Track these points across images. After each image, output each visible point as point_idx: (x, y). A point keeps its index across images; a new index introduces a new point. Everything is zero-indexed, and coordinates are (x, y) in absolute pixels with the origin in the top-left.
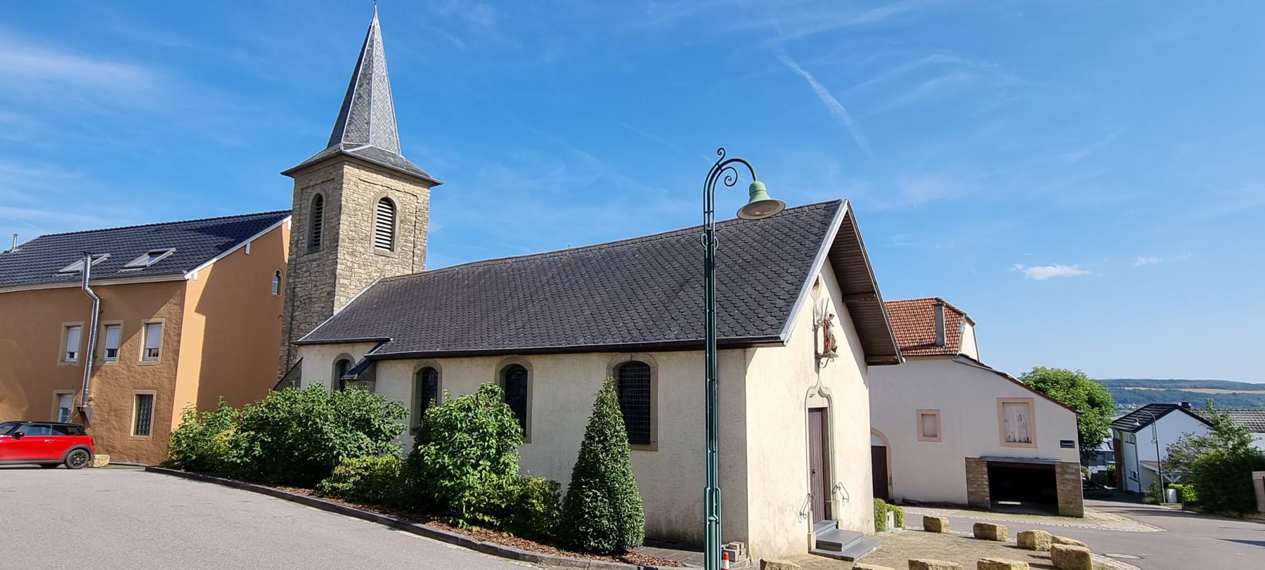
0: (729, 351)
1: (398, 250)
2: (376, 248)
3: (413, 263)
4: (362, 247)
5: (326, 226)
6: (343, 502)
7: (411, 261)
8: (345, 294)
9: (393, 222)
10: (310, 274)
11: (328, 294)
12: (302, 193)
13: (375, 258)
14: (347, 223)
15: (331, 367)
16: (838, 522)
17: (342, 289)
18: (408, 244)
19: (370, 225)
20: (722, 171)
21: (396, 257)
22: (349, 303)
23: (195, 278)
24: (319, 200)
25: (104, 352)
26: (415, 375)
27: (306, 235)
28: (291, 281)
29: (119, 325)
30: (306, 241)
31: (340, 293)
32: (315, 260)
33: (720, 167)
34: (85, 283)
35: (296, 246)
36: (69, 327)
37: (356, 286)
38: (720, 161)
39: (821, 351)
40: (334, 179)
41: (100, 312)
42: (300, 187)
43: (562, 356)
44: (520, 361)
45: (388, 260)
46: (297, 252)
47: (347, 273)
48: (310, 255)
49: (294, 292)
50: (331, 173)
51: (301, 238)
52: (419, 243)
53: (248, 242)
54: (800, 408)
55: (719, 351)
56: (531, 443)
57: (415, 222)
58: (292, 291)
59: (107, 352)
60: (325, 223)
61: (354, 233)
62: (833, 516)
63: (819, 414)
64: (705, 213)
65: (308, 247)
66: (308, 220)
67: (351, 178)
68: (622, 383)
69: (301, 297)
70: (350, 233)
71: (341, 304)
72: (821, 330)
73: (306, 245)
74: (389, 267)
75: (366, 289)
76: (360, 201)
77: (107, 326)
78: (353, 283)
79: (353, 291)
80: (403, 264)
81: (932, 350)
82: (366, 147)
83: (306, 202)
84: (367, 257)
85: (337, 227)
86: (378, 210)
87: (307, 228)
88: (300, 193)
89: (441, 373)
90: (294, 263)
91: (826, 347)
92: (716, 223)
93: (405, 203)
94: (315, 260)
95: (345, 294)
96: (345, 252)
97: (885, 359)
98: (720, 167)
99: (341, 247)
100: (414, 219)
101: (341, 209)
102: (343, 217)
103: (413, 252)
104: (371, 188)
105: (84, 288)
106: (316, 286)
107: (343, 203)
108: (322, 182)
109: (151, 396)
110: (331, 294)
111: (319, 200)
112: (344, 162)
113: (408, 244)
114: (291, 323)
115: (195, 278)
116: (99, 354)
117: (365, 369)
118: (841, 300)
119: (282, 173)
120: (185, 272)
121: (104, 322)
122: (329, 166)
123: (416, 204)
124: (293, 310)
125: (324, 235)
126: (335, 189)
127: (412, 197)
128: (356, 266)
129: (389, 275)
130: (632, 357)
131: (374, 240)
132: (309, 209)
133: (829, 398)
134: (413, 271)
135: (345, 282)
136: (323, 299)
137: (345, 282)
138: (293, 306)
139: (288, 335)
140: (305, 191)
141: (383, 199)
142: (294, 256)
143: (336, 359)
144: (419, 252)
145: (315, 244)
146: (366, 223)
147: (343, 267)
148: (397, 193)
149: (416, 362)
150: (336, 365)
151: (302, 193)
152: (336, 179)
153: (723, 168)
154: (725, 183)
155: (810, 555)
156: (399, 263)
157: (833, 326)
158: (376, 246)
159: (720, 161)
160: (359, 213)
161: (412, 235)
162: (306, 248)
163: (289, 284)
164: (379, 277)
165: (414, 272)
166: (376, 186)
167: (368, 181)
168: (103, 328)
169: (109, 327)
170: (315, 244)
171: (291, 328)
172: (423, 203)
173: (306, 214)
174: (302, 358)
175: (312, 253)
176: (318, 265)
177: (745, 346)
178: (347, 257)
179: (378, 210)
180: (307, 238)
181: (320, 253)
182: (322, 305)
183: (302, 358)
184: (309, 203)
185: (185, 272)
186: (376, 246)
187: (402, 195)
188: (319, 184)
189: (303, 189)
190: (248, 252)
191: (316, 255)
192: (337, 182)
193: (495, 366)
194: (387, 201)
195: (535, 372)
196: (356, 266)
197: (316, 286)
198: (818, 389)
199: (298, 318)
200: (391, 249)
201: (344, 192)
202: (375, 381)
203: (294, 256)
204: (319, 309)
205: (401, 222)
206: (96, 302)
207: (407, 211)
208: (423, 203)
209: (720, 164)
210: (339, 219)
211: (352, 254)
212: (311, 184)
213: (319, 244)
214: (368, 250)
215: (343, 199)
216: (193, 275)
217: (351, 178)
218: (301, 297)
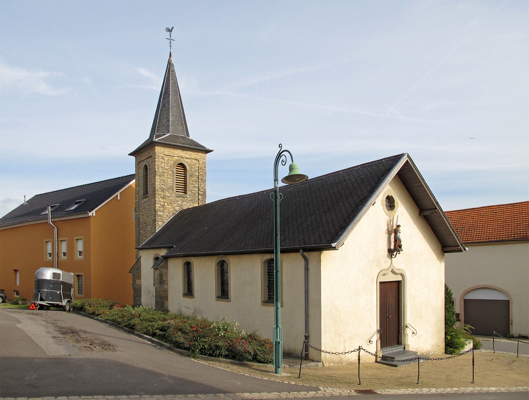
0: (314, 252)
1: (189, 192)
2: (177, 193)
3: (199, 200)
4: (169, 193)
5: (150, 183)
6: (46, 323)
7: (197, 199)
8: (161, 220)
9: (185, 177)
10: (145, 210)
11: (153, 221)
12: (139, 165)
13: (176, 199)
14: (159, 180)
15: (152, 260)
16: (405, 346)
17: (160, 218)
18: (195, 189)
19: (172, 180)
20: (281, 157)
21: (189, 197)
22: (164, 225)
23: (94, 215)
24: (146, 168)
25: (61, 254)
26: (183, 265)
27: (142, 188)
28: (137, 214)
29: (66, 240)
30: (142, 192)
31: (159, 220)
32: (146, 202)
33: (280, 155)
34: (49, 220)
35: (138, 195)
36: (47, 242)
37: (167, 216)
38: (280, 151)
39: (392, 247)
40: (151, 156)
41: (58, 234)
42: (137, 162)
43: (242, 256)
44: (225, 258)
45: (183, 199)
46: (139, 198)
47: (162, 208)
48: (145, 200)
49: (139, 220)
50: (150, 153)
51: (140, 190)
52: (201, 188)
53: (118, 193)
54: (372, 282)
55: (281, 254)
56: (231, 302)
57: (198, 175)
58: (138, 219)
59: (63, 254)
60: (149, 181)
61: (163, 186)
62: (403, 343)
63: (397, 283)
64: (274, 180)
65: (143, 195)
66: (142, 180)
67: (160, 154)
68: (269, 270)
69: (142, 222)
70: (161, 186)
71: (160, 225)
72: (393, 235)
73: (142, 194)
74: (185, 203)
75: (172, 217)
76: (166, 167)
77: (61, 241)
78: (165, 214)
79: (165, 219)
80: (193, 201)
81: (495, 239)
82: (168, 135)
83: (141, 169)
84: (172, 199)
85: (154, 184)
86: (176, 171)
87: (142, 184)
88: (138, 164)
89: (193, 264)
90: (138, 204)
91: (395, 246)
92: (279, 187)
93: (192, 165)
94: (146, 202)
95: (161, 220)
96: (160, 197)
97: (453, 248)
98: (280, 155)
99: (157, 194)
100: (198, 174)
101: (155, 173)
102: (157, 178)
103: (198, 193)
104: (171, 159)
105: (50, 222)
106: (148, 216)
107: (156, 169)
108: (147, 158)
109: (82, 275)
110: (155, 221)
111: (146, 168)
112: (155, 146)
113: (195, 189)
114: (139, 237)
115: (94, 215)
116: (59, 255)
117: (162, 262)
118: (419, 214)
119: (129, 155)
120: (88, 212)
121: (60, 239)
122: (149, 149)
123: (198, 165)
124: (139, 229)
125: (149, 188)
126: (152, 162)
127: (195, 161)
128: (166, 204)
129: (185, 208)
130: (271, 256)
131: (175, 188)
132: (142, 174)
133: (402, 275)
134: (199, 204)
135: (161, 213)
136: (151, 223)
137: (161, 213)
138: (139, 228)
139: (138, 243)
140: (140, 163)
141: (179, 164)
142: (137, 200)
143: (153, 258)
144: (202, 193)
145: (146, 192)
146: (170, 180)
147: (159, 205)
148: (187, 160)
149: (183, 258)
150: (154, 259)
151: (139, 165)
152: (152, 156)
153: (281, 155)
154: (283, 165)
155: (376, 363)
156: (190, 200)
157: (400, 233)
158: (176, 192)
159: (280, 151)
160: (166, 174)
161: (197, 183)
162: (142, 195)
163: (136, 216)
164: (179, 209)
165: (200, 205)
166: (175, 157)
167: (169, 155)
168: (59, 242)
169: (62, 242)
170: (146, 192)
171: (139, 239)
172: (202, 164)
173: (141, 177)
174: (141, 256)
175: (145, 198)
176: (148, 205)
177: (320, 249)
178: (161, 199)
179: (176, 171)
180: (142, 190)
181: (148, 198)
182: (151, 227)
183: (141, 256)
184: (142, 170)
185: (88, 212)
186: (176, 192)
187: (190, 161)
188: (145, 159)
189: (139, 163)
190: (119, 199)
191: (146, 199)
192: (152, 157)
193: (214, 261)
194: (182, 165)
195: (231, 264)
196: (166, 204)
197: (148, 216)
198: (391, 269)
199: (141, 234)
200: (185, 193)
201: (156, 163)
202: (167, 269)
203: (137, 200)
204: (150, 229)
205: (190, 176)
206: (55, 229)
207: (193, 169)
208: (202, 164)
209: (280, 152)
210: (155, 179)
211: (163, 198)
212: (142, 159)
213: (147, 193)
214: (171, 195)
215: (156, 167)
216: (93, 214)
217: (160, 154)
218: (142, 222)
